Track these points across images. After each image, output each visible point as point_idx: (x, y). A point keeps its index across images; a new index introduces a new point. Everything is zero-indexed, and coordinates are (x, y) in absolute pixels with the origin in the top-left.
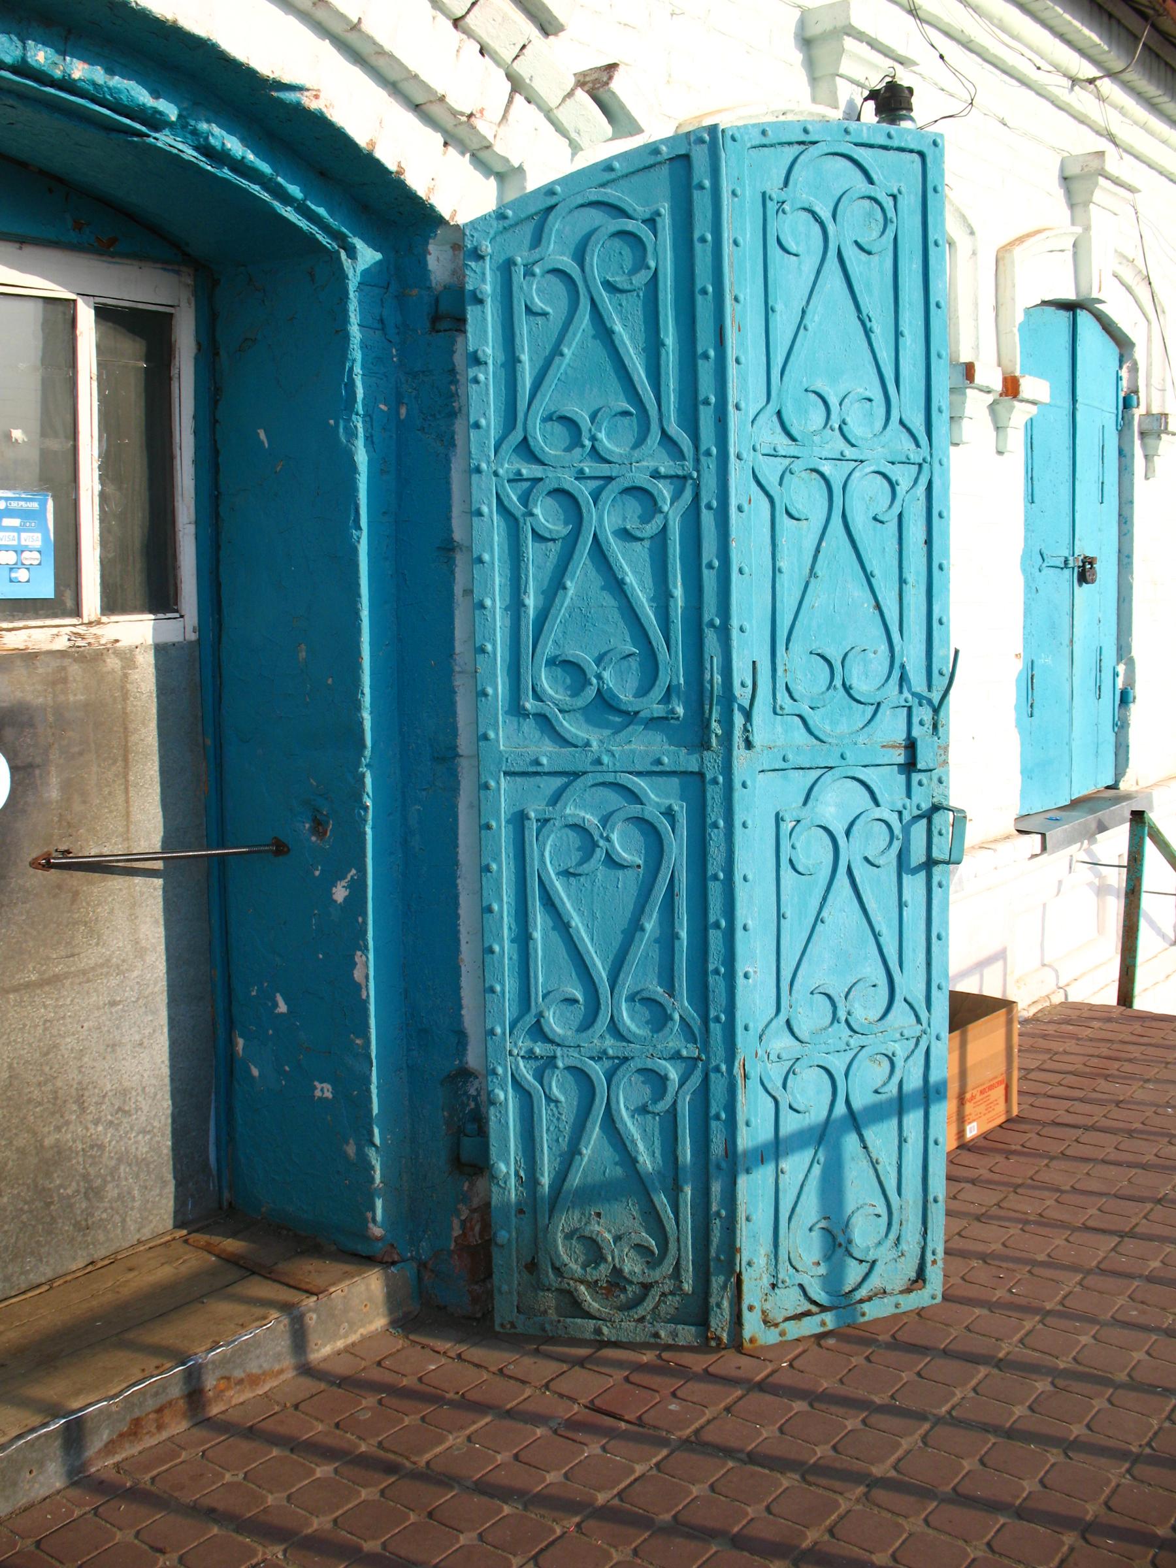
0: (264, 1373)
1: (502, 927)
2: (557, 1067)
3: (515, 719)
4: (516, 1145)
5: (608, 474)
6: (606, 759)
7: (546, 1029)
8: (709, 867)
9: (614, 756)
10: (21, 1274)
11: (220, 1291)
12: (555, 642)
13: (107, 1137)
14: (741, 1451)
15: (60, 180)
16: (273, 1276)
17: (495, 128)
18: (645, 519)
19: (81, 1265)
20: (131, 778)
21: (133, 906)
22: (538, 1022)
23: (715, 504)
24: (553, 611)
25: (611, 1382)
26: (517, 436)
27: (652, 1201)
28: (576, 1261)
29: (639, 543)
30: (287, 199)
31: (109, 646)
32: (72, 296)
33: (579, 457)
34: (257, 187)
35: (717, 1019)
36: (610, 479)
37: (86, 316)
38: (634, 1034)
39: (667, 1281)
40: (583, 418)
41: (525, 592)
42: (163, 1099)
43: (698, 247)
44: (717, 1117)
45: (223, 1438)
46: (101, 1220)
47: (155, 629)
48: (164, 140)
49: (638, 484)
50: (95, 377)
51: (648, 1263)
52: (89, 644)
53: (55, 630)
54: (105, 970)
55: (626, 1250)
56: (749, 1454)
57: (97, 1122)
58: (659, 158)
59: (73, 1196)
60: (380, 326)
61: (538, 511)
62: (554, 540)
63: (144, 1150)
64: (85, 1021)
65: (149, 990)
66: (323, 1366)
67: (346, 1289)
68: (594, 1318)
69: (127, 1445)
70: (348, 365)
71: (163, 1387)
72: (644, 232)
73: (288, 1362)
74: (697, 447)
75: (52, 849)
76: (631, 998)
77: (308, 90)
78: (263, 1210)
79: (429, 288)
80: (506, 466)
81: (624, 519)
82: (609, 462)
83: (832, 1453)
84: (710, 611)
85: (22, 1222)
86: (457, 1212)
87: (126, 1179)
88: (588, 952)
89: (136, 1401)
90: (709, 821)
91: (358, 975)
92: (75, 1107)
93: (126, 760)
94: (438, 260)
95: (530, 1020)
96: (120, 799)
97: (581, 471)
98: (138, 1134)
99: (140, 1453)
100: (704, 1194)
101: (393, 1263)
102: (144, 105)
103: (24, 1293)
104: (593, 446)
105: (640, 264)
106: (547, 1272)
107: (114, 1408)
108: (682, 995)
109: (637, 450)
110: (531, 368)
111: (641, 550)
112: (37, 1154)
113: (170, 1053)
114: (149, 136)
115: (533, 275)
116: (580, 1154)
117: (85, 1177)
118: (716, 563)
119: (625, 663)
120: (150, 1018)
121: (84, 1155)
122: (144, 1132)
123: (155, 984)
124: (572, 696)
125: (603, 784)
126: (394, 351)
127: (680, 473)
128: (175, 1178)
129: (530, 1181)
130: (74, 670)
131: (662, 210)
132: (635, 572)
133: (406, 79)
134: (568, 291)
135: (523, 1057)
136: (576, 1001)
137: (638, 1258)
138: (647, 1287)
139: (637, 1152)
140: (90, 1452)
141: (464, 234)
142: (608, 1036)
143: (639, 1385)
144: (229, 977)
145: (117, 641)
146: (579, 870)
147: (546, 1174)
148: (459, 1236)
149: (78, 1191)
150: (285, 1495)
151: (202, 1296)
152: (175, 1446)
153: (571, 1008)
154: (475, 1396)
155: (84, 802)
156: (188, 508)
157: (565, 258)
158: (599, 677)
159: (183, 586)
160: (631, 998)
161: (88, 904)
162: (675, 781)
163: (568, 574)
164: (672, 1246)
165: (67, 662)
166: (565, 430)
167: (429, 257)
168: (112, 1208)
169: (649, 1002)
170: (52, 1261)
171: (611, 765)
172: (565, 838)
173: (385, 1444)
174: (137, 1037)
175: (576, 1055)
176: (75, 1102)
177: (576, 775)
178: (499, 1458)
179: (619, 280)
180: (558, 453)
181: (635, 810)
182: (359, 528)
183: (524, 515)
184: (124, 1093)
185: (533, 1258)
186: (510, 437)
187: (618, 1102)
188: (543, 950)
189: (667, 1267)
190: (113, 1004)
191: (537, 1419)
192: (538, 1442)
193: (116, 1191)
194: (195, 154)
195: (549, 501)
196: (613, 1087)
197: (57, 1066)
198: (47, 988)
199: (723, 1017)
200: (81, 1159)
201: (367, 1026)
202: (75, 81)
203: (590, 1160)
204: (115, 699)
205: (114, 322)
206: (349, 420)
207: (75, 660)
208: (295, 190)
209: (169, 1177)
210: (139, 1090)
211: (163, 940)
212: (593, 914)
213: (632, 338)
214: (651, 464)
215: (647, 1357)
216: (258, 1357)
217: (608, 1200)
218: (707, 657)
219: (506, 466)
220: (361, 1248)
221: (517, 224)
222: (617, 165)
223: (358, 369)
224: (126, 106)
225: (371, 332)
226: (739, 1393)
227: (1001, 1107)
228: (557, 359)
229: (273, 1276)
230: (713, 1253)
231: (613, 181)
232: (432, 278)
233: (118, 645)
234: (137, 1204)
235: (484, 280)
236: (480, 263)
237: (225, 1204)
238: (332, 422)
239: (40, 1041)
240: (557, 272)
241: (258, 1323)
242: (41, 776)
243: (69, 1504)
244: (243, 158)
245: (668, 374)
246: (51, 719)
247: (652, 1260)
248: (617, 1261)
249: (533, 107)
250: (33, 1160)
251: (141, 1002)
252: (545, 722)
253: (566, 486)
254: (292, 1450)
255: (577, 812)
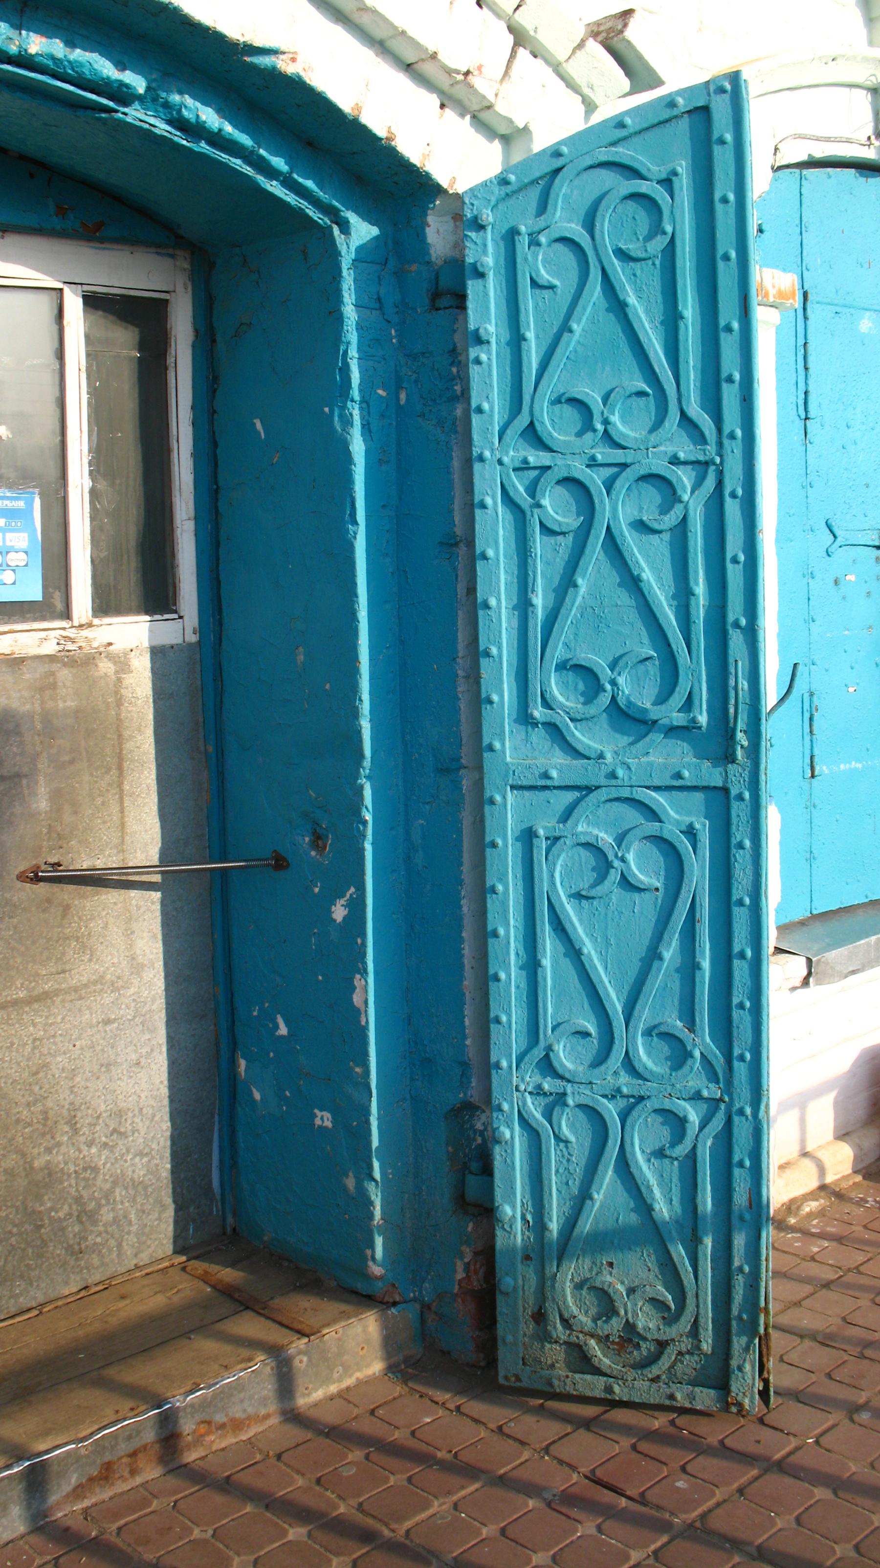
0: (249, 1418)
1: (508, 953)
2: (566, 1105)
3: (523, 727)
4: (523, 1187)
5: (623, 461)
6: (620, 773)
7: (556, 1064)
8: (734, 891)
9: (629, 768)
10: (11, 1297)
11: (203, 1328)
12: (566, 644)
13: (101, 1159)
14: (749, 1544)
15: (41, 164)
16: (266, 1312)
17: (497, 86)
18: (665, 509)
19: (75, 1290)
20: (126, 787)
21: (129, 920)
22: (547, 1056)
23: (740, 492)
24: (563, 611)
25: (617, 1449)
26: (523, 421)
27: (668, 1253)
28: (586, 1312)
29: (657, 536)
30: (271, 173)
31: (102, 649)
32: (59, 285)
33: (591, 443)
34: (239, 161)
35: (742, 1058)
36: (624, 466)
37: (74, 304)
38: (651, 1072)
39: (684, 1338)
40: (595, 400)
41: (533, 591)
42: (162, 1120)
43: (719, 207)
44: (741, 1164)
45: (196, 1488)
46: (95, 1244)
47: (150, 631)
48: (134, 114)
49: (655, 470)
50: (84, 369)
51: (664, 1318)
52: (80, 648)
53: (43, 634)
54: (99, 987)
55: (640, 1304)
56: (759, 1548)
57: (90, 1144)
58: (675, 112)
59: (65, 1219)
60: (377, 306)
61: (546, 502)
62: (563, 534)
63: (142, 1173)
64: (76, 1039)
65: (147, 1008)
66: (313, 1413)
67: (341, 1331)
68: (605, 1375)
69: (97, 1490)
70: (342, 348)
71: (137, 1429)
72: (659, 193)
73: (272, 1407)
74: (719, 430)
75: (40, 861)
76: (648, 1033)
77: (283, 53)
78: (266, 1238)
79: (429, 263)
80: (512, 453)
81: (641, 509)
82: (624, 448)
83: (853, 1554)
84: (735, 611)
85: (11, 1245)
86: (461, 1255)
87: (122, 1203)
88: (602, 982)
89: (107, 1444)
90: (734, 842)
91: (357, 999)
92: (66, 1128)
93: (120, 768)
94: (438, 232)
95: (538, 1053)
96: (115, 809)
97: (593, 458)
98: (135, 1156)
99: (111, 1498)
100: (725, 1248)
101: (395, 1304)
102: (108, 78)
103: (12, 1317)
104: (606, 430)
105: (656, 229)
106: (555, 1323)
107: (83, 1452)
108: (703, 1029)
109: (654, 434)
110: (538, 346)
111: (661, 545)
112: (26, 1175)
113: (169, 1073)
114: (117, 111)
115: (539, 244)
116: (591, 1198)
117: (78, 1200)
118: (742, 558)
119: (642, 667)
120: (147, 1036)
121: (77, 1178)
122: (141, 1154)
123: (153, 1001)
124: (584, 704)
125: (618, 799)
126: (393, 332)
127: (701, 458)
128: (175, 1202)
129: (539, 1225)
130: (64, 675)
131: (679, 170)
132: (653, 569)
133: (393, 37)
134: (578, 262)
135: (530, 1093)
136: (587, 1034)
137: (654, 1312)
138: (662, 1345)
139: (653, 1199)
140: (53, 1499)
141: (463, 203)
142: (622, 1073)
143: (646, 1455)
144: (232, 994)
145: (110, 644)
146: (593, 893)
147: (555, 1219)
148: (463, 1279)
149: (70, 1214)
150: (252, 1558)
151: (192, 1331)
152: (149, 1491)
153: (582, 1041)
154: (467, 1457)
155: (76, 813)
156: (187, 503)
157: (573, 225)
158: (613, 683)
159: (182, 585)
160: (648, 1033)
161: (80, 918)
162: (699, 796)
163: (579, 570)
164: (690, 1301)
165: (55, 667)
166: (576, 411)
167: (428, 230)
168: (107, 1232)
169: (669, 1037)
170: (43, 1285)
171: (626, 778)
172: (577, 859)
173: (366, 1507)
174: (134, 1057)
175: (588, 1092)
176: (66, 1123)
177: (589, 789)
178: (485, 1531)
179: (633, 248)
180: (567, 438)
181: (653, 828)
182: (355, 523)
183: (532, 506)
184: (120, 1114)
185: (541, 1308)
186: (516, 422)
187: (632, 1144)
188: (552, 978)
189: (684, 1324)
190: (107, 1022)
191: (530, 1489)
192: (530, 1514)
193: (111, 1215)
194: (169, 128)
195: (560, 490)
196: (628, 1128)
197: (47, 1086)
198: (36, 1006)
199: (748, 1056)
200: (73, 1182)
201: (366, 1054)
202: (31, 55)
203: (601, 1206)
204: (108, 705)
205: (104, 311)
206: (344, 407)
207: (65, 665)
208: (279, 163)
209: (169, 1201)
210: (136, 1112)
211: (161, 956)
212: (607, 940)
213: (647, 311)
214: (669, 449)
215: (659, 1422)
216: (242, 1401)
217: (622, 1250)
218: (731, 660)
219: (512, 453)
220: (360, 1286)
221: (520, 190)
222: (628, 121)
223: (353, 352)
224: (89, 80)
225: (368, 312)
226: (755, 1472)
227: (824, 1327)
228: (566, 335)
229: (266, 1312)
230: (735, 1311)
231: (625, 139)
232: (432, 252)
233: (111, 648)
234: (134, 1228)
235: (485, 252)
236: (481, 233)
237: (229, 1229)
238: (327, 409)
239: (28, 1060)
240: (563, 240)
241: (243, 1366)
242: (29, 787)
243: (31, 1551)
244: (220, 130)
245: (687, 350)
246: (39, 727)
247: (671, 1317)
248: (630, 1315)
249: (539, 62)
250: (21, 1183)
251: (138, 1020)
252: (554, 730)
253: (576, 475)
254: (267, 1507)
255: (590, 829)
